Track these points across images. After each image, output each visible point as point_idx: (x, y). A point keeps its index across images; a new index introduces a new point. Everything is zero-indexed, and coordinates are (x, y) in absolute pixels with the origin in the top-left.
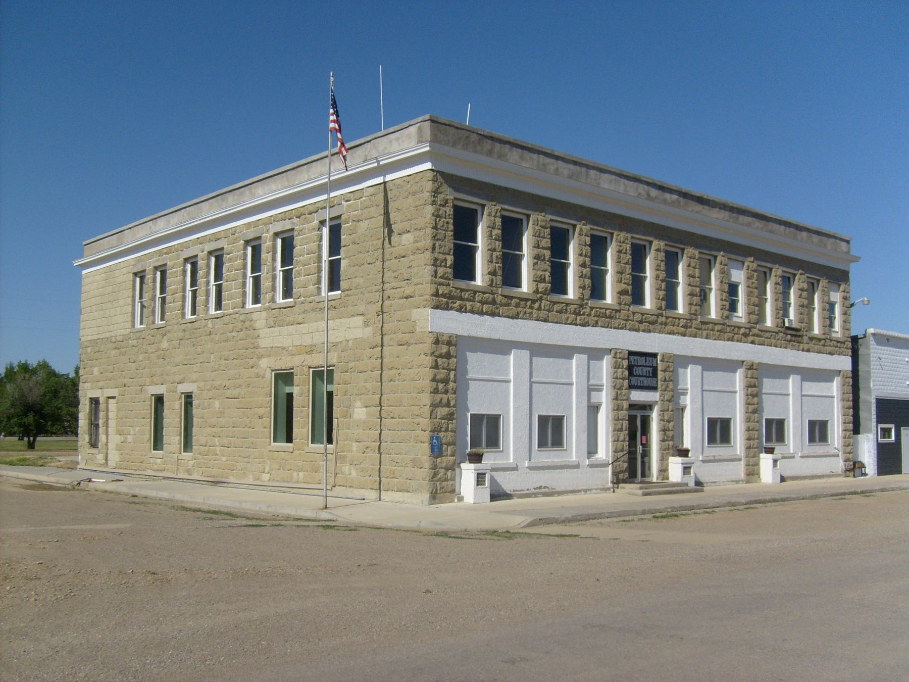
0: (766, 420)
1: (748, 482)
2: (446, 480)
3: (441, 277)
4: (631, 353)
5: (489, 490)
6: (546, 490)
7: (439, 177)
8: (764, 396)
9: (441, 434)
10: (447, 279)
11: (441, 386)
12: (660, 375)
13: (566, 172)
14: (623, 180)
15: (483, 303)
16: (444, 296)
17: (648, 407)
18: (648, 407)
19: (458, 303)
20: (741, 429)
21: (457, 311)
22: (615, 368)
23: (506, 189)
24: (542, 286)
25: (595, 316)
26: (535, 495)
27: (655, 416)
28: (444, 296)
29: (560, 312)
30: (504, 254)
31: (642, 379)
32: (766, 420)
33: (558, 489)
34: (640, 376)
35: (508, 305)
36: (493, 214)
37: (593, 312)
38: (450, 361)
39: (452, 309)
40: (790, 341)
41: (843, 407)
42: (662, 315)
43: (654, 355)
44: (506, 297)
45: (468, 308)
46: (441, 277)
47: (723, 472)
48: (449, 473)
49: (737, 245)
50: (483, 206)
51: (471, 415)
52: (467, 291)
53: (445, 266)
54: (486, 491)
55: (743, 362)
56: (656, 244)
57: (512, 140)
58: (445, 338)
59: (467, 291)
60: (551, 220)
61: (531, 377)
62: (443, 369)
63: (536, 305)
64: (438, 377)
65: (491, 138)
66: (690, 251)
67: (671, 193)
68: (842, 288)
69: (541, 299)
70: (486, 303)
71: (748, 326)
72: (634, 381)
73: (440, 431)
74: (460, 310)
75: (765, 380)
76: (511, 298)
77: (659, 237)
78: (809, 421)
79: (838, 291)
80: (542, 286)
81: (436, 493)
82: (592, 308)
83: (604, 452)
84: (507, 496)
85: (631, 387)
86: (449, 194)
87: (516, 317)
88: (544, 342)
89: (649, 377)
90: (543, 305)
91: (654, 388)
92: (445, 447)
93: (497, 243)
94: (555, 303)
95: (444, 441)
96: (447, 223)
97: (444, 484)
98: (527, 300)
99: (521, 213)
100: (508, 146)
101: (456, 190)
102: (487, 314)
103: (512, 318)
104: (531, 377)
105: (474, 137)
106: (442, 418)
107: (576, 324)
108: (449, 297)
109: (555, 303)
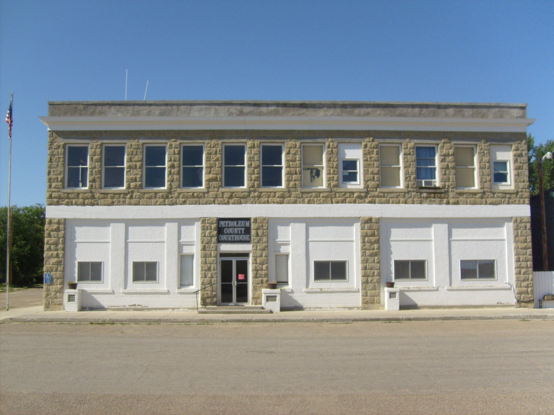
0: (80, 263)
1: (364, 308)
2: (56, 298)
3: (55, 188)
4: (220, 220)
5: (398, 301)
6: (139, 307)
7: (54, 134)
8: (391, 242)
9: (53, 273)
10: (58, 188)
11: (52, 247)
12: (253, 232)
13: (157, 112)
14: (213, 107)
15: (84, 199)
16: (55, 198)
17: (247, 255)
18: (247, 255)
19: (66, 200)
20: (357, 268)
21: (65, 205)
22: (203, 229)
23: (106, 132)
24: (371, 184)
25: (183, 198)
26: (127, 309)
27: (250, 260)
28: (55, 198)
29: (150, 198)
30: (417, 168)
31: (233, 236)
32: (80, 263)
33: (150, 307)
34: (231, 234)
35: (104, 198)
36: (94, 147)
37: (181, 196)
38: (60, 233)
39: (62, 204)
40: (427, 198)
41: (516, 248)
42: (255, 191)
43: (248, 219)
44: (102, 194)
45: (74, 203)
46: (55, 188)
47: (341, 299)
48: (58, 294)
49: (144, 131)
50: (476, 145)
51: (79, 262)
52: (73, 193)
53: (57, 181)
54: (396, 301)
55: (512, 218)
56: (249, 143)
57: (110, 102)
58: (56, 221)
59: (73, 193)
60: (455, 144)
61: (179, 237)
62: (54, 237)
63: (128, 196)
64: (50, 242)
65: (95, 105)
66: (290, 143)
67: (367, 107)
68: (514, 147)
69: (133, 192)
70: (87, 198)
71: (481, 191)
72: (223, 237)
73: (52, 271)
74: (67, 204)
75: (392, 230)
76: (107, 194)
77: (250, 138)
78: (134, 263)
79: (509, 151)
80: (371, 184)
81: (49, 304)
82: (180, 194)
83: (196, 285)
84: (414, 307)
85: (219, 241)
86: (61, 141)
87: (112, 204)
88: (135, 217)
89: (241, 234)
90: (134, 196)
91: (248, 242)
92: (55, 280)
93: (97, 164)
94: (144, 193)
95: (54, 277)
96: (59, 158)
97: (55, 300)
98: (513, 193)
99: (471, 144)
100: (108, 106)
101: (64, 138)
102: (87, 205)
103: (108, 205)
104: (179, 237)
105: (81, 107)
106: (53, 264)
107: (165, 205)
108: (59, 198)
109: (144, 193)
